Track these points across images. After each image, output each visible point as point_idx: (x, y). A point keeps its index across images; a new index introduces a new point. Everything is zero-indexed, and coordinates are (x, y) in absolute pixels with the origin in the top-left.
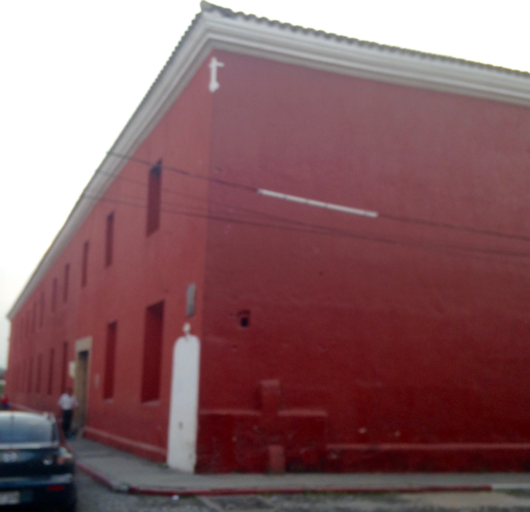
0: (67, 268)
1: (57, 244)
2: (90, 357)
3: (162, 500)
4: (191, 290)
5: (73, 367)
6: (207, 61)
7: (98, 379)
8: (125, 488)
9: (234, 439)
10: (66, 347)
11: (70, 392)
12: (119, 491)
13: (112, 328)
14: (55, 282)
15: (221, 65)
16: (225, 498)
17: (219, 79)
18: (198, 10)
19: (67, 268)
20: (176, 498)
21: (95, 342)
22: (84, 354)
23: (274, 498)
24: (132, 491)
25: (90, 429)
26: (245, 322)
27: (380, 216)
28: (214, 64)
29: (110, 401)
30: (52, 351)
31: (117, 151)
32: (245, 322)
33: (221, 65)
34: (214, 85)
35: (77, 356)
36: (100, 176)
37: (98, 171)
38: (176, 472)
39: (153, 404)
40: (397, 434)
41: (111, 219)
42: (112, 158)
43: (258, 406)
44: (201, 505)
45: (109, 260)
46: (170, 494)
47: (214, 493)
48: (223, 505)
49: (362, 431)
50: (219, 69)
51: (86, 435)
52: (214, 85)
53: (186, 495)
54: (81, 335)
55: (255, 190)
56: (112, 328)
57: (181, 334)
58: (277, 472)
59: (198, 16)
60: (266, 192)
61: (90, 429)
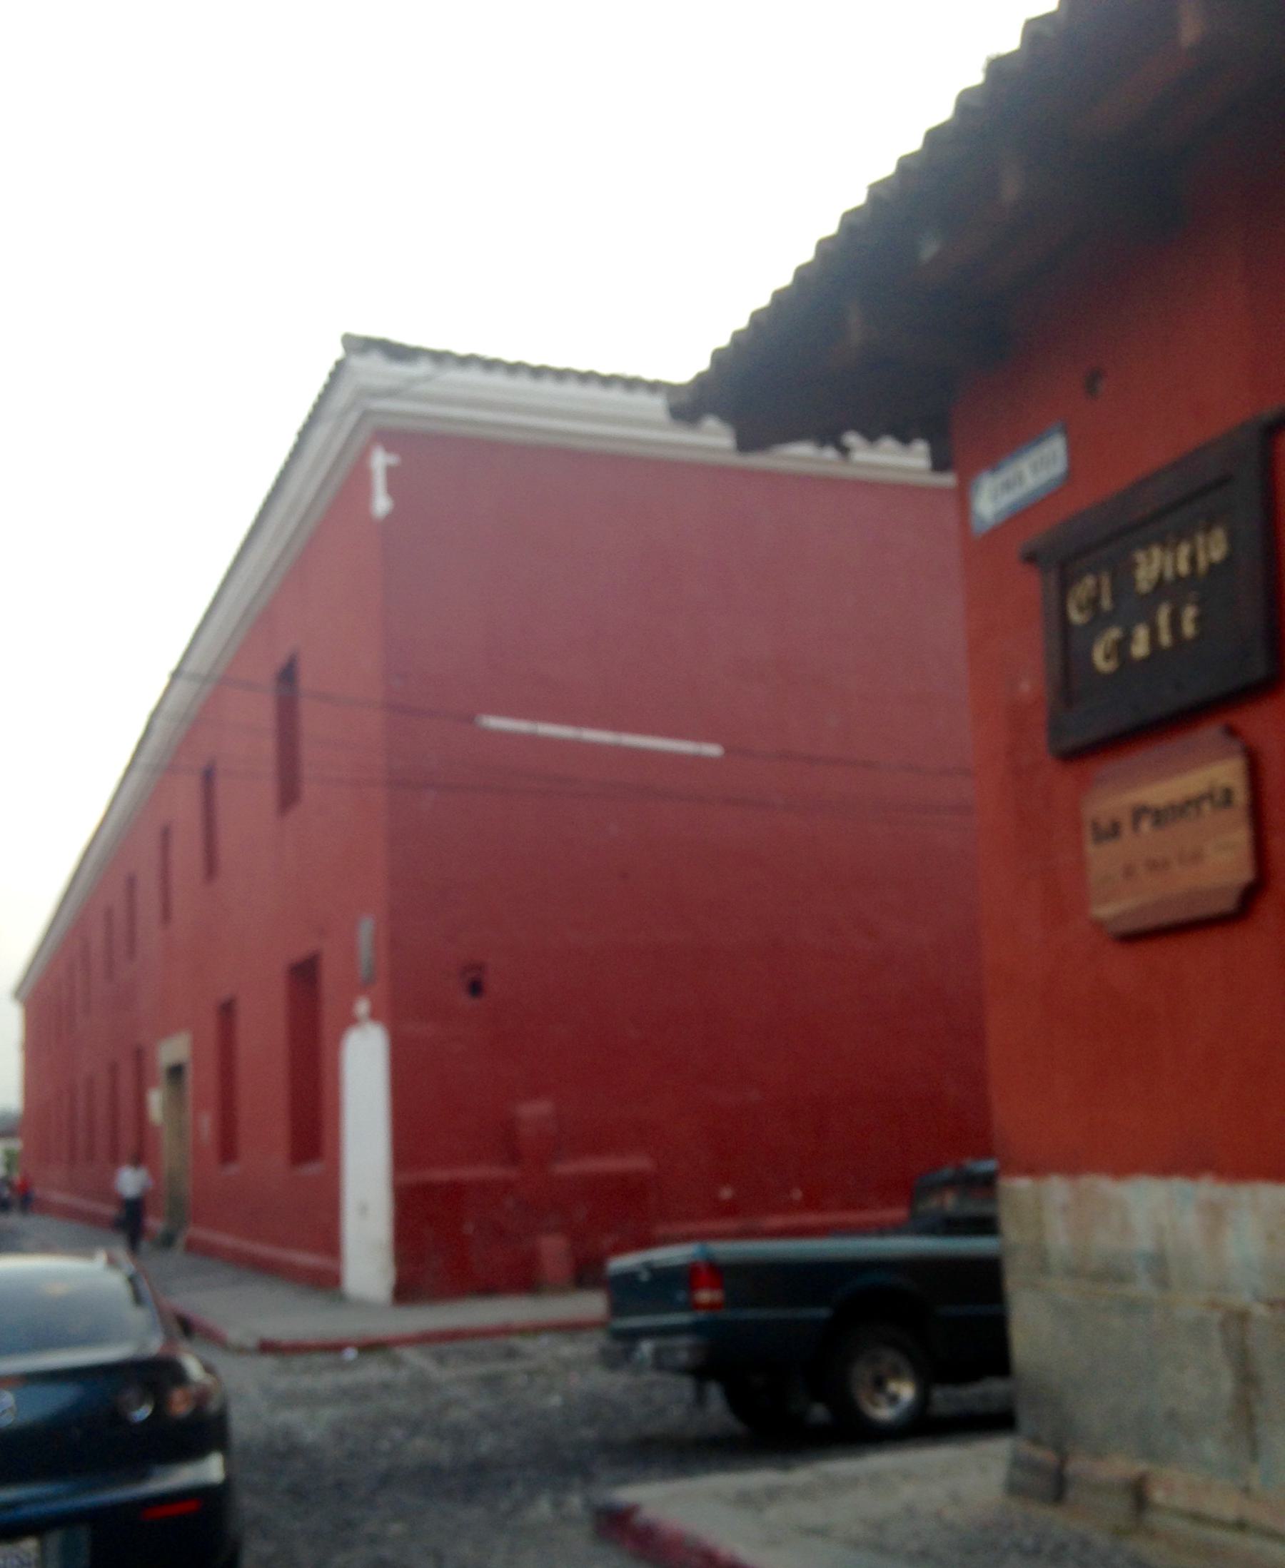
0: (131, 883)
1: (115, 816)
2: (189, 1076)
3: (319, 1359)
4: (366, 930)
5: (156, 1101)
6: (365, 455)
7: (207, 1123)
8: (251, 1342)
9: (469, 1228)
10: (140, 1057)
11: (138, 1159)
12: (241, 1350)
13: (227, 1011)
14: (109, 913)
15: (393, 460)
16: (446, 1347)
17: (392, 490)
18: (338, 352)
19: (131, 883)
20: (350, 1354)
21: (196, 1046)
22: (176, 1072)
23: (545, 1340)
24: (267, 1348)
25: (196, 1232)
26: (476, 988)
27: (728, 750)
28: (380, 461)
29: (233, 1169)
30: (113, 1069)
31: (190, 667)
32: (476, 988)
33: (393, 460)
34: (381, 504)
35: (162, 1076)
36: (181, 685)
37: (176, 675)
38: (363, 1305)
39: (312, 1169)
40: (797, 1194)
41: (208, 777)
42: (181, 685)
43: (514, 1156)
44: (397, 1363)
45: (166, 914)
46: (336, 1348)
47: (424, 1339)
48: (441, 1359)
49: (726, 1193)
50: (391, 472)
51: (192, 1246)
52: (381, 504)
53: (370, 1347)
54: (167, 1031)
55: (470, 719)
56: (227, 1011)
57: (350, 1021)
58: (559, 1289)
59: (340, 366)
60: (495, 723)
61: (196, 1232)
